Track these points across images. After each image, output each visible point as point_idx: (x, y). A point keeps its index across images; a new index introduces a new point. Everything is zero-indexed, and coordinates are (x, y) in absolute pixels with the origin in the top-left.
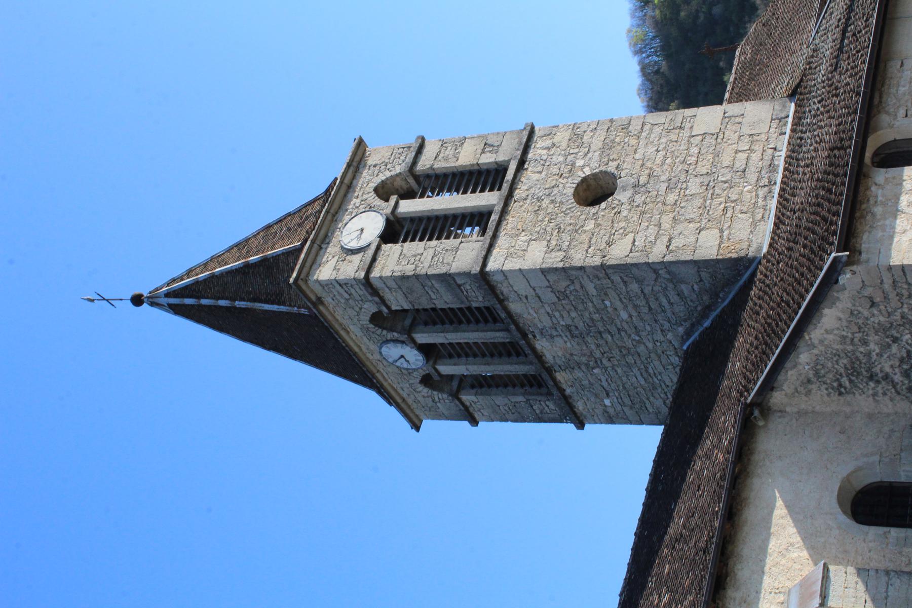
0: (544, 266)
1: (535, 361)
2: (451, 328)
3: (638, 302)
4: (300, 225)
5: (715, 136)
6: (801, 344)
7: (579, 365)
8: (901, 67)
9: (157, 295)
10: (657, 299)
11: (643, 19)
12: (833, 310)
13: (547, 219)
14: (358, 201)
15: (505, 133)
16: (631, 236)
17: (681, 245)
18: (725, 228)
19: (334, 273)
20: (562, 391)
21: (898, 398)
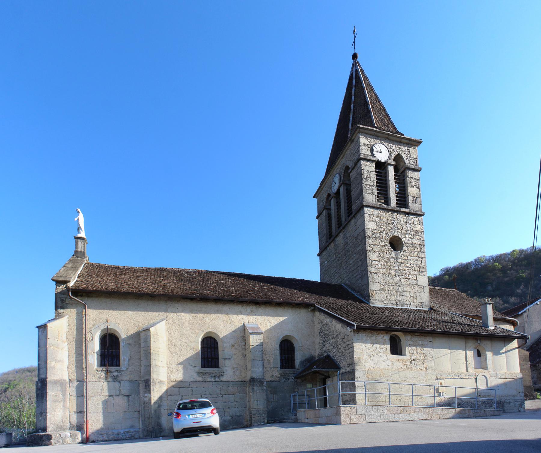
0: (366, 229)
1: (336, 234)
2: (346, 200)
3: (355, 266)
4: (384, 124)
5: (416, 284)
6: (331, 319)
7: (336, 250)
8: (429, 341)
9: (356, 66)
10: (356, 272)
11: (489, 260)
12: (341, 327)
13: (385, 227)
14: (394, 148)
15: (421, 205)
16: (378, 259)
17: (374, 277)
18: (381, 291)
19: (363, 144)
20: (328, 246)
21: (319, 350)
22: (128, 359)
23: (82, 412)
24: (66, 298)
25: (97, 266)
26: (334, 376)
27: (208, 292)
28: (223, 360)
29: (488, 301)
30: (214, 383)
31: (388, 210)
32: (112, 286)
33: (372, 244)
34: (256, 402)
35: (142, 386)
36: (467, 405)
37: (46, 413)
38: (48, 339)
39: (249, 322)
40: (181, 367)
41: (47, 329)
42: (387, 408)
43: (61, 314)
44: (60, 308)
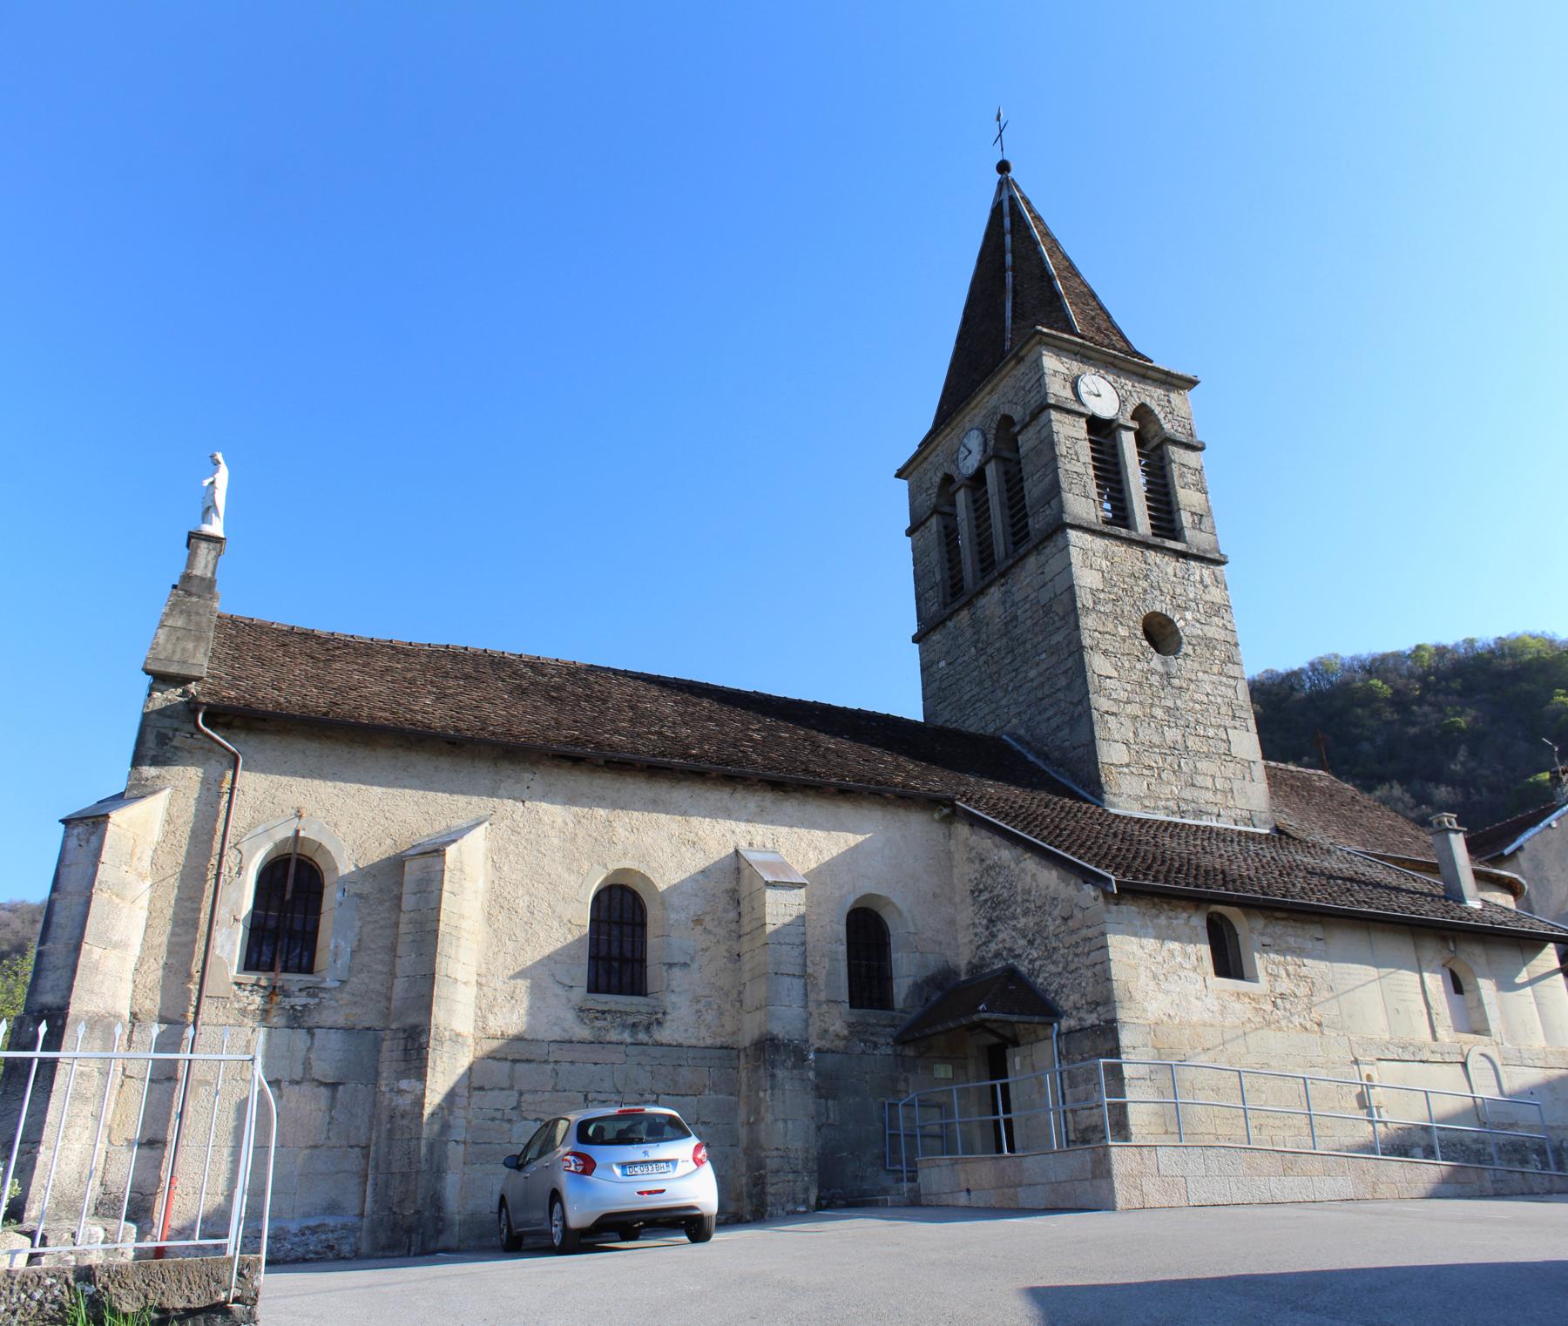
0: (1077, 588)
1: (978, 588)
3: (1046, 687)
7: (977, 632)
10: (1052, 705)
11: (1351, 669)
14: (1130, 388)
16: (1115, 674)
19: (1051, 372)
20: (950, 618)
21: (973, 947)
22: (349, 949)
23: (158, 1142)
24: (176, 730)
25: (245, 624)
26: (1038, 1040)
27: (616, 738)
28: (664, 968)
29: (1450, 823)
30: (631, 1050)
31: (1131, 542)
32: (318, 700)
33: (1096, 630)
34: (780, 1125)
35: (390, 1051)
36: (1455, 1153)
37: (39, 1142)
38: (101, 866)
39: (751, 844)
40: (522, 985)
41: (106, 829)
42: (1243, 1154)
43: (149, 783)
44: (150, 762)
